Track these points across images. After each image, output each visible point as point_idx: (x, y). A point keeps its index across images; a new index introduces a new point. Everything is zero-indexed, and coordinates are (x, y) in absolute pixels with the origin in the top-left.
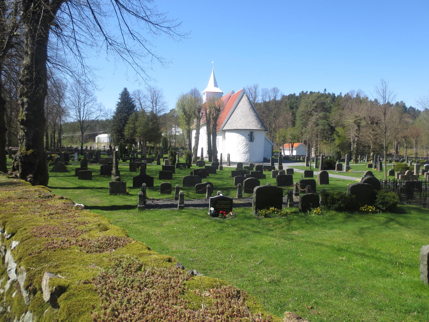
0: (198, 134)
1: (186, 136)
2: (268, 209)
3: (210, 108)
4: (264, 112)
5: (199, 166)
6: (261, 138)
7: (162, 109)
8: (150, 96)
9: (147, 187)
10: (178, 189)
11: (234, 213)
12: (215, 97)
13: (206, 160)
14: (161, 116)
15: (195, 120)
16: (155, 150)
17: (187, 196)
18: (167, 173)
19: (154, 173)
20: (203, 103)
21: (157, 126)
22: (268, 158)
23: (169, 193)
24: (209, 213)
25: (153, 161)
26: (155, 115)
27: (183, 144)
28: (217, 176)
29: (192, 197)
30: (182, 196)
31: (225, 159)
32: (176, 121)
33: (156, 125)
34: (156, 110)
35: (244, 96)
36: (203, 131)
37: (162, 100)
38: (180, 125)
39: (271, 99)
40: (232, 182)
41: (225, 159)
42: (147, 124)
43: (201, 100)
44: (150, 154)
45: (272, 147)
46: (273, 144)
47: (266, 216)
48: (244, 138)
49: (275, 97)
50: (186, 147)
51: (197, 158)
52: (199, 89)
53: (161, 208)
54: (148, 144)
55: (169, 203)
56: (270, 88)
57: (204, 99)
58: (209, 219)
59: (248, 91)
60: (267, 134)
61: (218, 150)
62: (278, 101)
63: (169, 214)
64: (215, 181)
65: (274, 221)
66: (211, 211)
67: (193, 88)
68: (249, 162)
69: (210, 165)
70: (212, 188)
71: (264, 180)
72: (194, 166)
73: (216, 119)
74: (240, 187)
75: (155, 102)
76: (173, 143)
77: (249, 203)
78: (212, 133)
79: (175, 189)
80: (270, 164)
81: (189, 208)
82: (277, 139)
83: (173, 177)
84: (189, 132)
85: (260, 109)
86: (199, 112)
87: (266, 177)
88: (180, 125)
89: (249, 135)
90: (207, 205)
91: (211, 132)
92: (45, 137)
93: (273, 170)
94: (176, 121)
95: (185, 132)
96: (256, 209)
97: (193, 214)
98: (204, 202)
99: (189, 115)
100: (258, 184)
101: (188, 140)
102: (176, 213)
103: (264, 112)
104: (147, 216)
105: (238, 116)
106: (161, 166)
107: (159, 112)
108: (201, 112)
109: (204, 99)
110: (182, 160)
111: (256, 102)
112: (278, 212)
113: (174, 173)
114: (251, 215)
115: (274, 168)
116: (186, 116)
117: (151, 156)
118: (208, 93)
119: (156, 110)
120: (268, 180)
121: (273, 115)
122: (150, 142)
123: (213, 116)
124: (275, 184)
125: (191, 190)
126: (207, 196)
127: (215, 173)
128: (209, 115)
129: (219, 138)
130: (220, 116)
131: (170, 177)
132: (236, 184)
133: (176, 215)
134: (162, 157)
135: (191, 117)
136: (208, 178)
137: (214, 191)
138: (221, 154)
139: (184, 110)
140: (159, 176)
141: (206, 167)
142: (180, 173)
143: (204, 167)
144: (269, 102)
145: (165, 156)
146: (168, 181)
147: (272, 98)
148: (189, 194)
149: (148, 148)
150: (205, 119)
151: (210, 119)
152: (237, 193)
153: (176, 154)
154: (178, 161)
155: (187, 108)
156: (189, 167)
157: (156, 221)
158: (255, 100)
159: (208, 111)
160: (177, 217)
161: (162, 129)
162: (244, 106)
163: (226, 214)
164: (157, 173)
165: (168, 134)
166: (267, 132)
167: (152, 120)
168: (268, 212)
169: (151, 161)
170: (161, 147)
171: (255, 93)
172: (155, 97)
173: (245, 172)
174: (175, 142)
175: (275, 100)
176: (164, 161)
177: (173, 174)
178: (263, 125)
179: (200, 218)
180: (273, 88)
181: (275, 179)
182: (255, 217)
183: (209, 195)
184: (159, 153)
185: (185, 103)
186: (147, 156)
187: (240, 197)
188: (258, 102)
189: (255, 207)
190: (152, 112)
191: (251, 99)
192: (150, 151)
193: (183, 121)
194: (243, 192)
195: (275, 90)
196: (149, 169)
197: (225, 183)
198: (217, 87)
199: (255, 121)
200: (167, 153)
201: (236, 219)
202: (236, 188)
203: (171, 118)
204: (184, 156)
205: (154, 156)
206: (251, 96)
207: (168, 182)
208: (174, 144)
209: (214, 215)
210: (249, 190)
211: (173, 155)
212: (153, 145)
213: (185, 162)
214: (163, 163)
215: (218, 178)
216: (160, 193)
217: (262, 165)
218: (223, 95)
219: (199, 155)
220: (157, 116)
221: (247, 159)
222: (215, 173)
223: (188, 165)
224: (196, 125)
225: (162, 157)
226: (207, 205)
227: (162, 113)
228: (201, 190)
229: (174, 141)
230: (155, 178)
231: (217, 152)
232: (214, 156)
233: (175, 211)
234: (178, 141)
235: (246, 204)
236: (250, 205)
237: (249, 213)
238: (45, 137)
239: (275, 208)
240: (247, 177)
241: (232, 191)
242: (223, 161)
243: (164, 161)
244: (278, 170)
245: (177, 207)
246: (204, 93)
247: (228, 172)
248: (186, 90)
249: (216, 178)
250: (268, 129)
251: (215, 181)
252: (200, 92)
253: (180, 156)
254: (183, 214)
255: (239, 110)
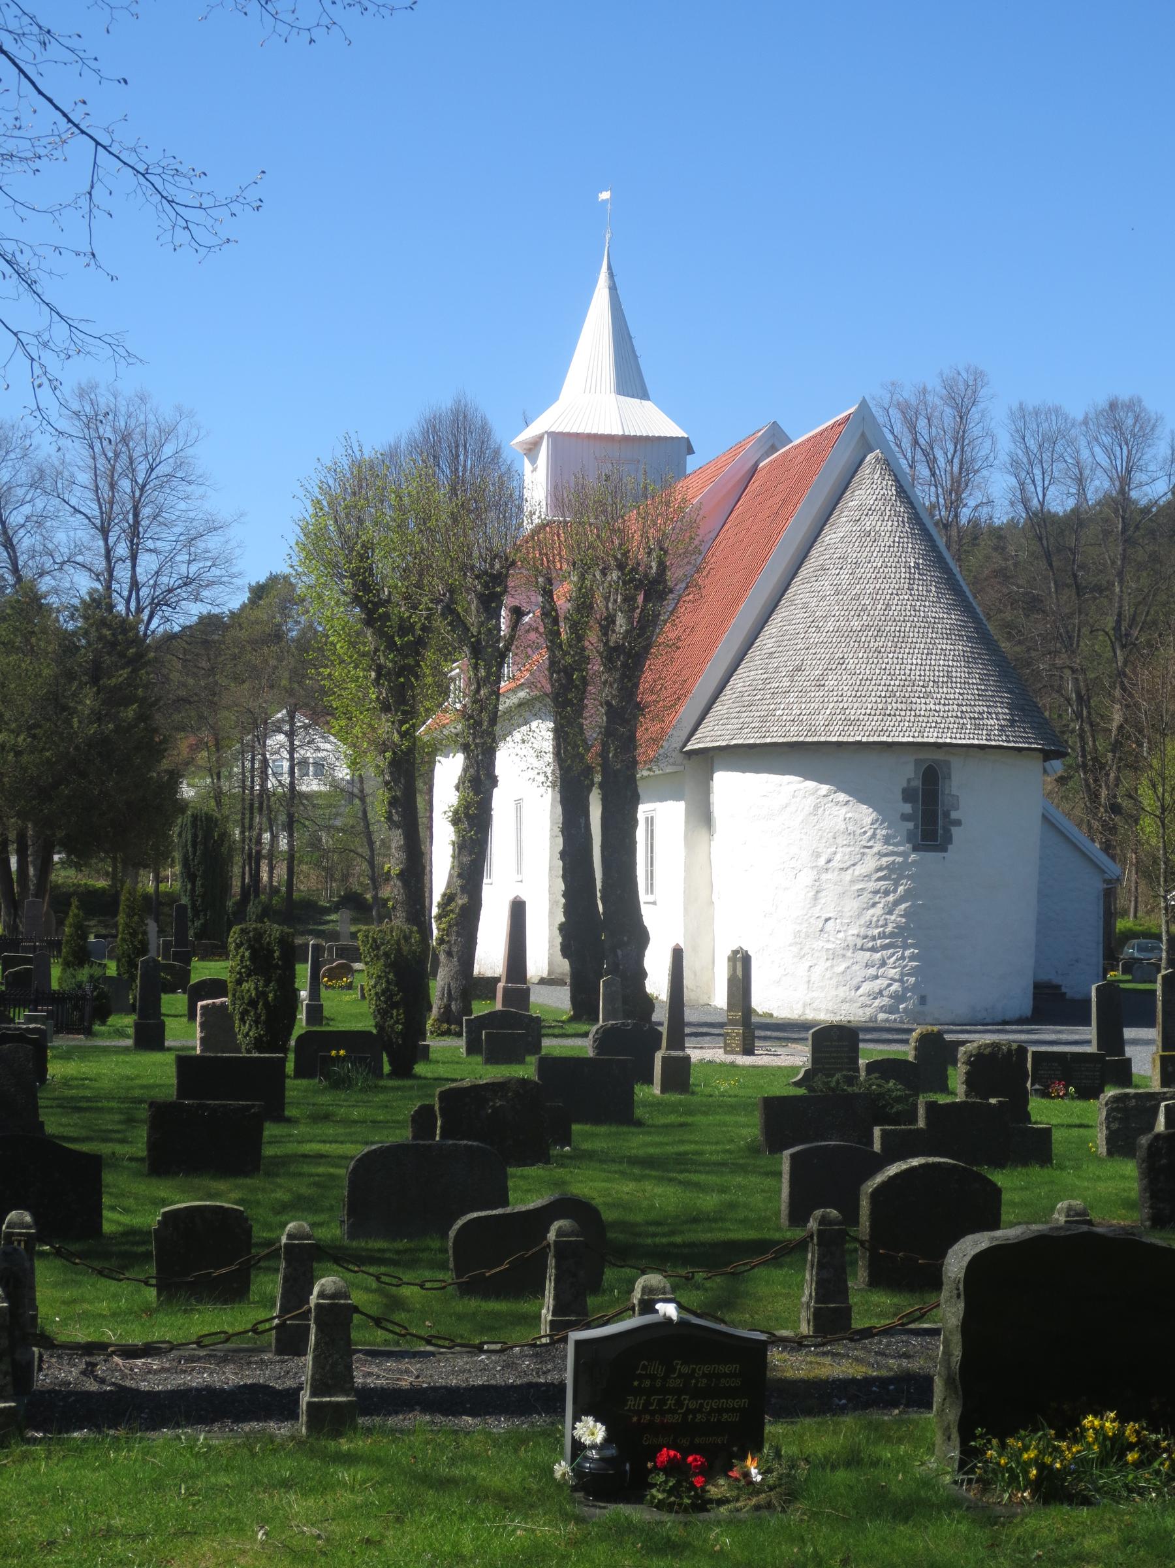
0: (480, 782)
1: (378, 808)
2: (1069, 1427)
3: (583, 568)
4: (1033, 604)
5: (491, 1060)
6: (1008, 817)
7: (187, 582)
8: (85, 478)
9: (40, 1238)
10: (304, 1260)
11: (780, 1469)
12: (611, 474)
13: (553, 1002)
14: (170, 637)
15: (458, 671)
16: (121, 918)
17: (378, 1322)
18: (215, 1118)
19: (109, 1122)
20: (528, 527)
21: (142, 717)
22: (1071, 990)
23: (233, 1290)
24: (562, 1469)
25: (102, 1014)
26: (125, 627)
27: (361, 867)
28: (637, 1143)
29: (425, 1328)
30: (337, 1317)
31: (714, 993)
32: (298, 676)
33: (130, 712)
34: (135, 585)
35: (865, 470)
36: (525, 766)
37: (183, 507)
38: (330, 712)
39: (1092, 497)
40: (769, 1193)
41: (714, 993)
42: (57, 704)
43: (508, 501)
44: (81, 956)
45: (1109, 894)
46: (1113, 869)
47: (1052, 1489)
48: (866, 815)
49: (1125, 481)
50: (386, 892)
51: (473, 986)
52: (491, 409)
53: (155, 1424)
54: (64, 875)
55: (229, 1377)
56: (1079, 399)
57: (536, 486)
58: (567, 1517)
59: (899, 427)
60: (1062, 780)
61: (650, 916)
62: (1146, 510)
63: (223, 1479)
64: (626, 1188)
65: (1113, 1538)
66: (578, 1446)
67: (444, 402)
68: (916, 1017)
69: (583, 1046)
70: (597, 1252)
71: (1036, 1173)
72: (449, 1058)
73: (629, 659)
74: (832, 1243)
75: (125, 518)
76: (277, 860)
77: (906, 1378)
78: (602, 786)
79: (275, 1254)
80: (1083, 1039)
81: (391, 1421)
82: (1148, 824)
83: (268, 1151)
84: (408, 775)
85: (1003, 575)
86: (490, 603)
87: (1057, 1148)
88: (330, 712)
89: (908, 795)
90: (541, 1400)
91: (589, 770)
92: (657, 1240)
93: (1110, 1092)
94: (298, 676)
95: (375, 767)
96: (966, 1431)
97: (425, 1480)
98: (525, 1370)
99: (405, 628)
100: (986, 1212)
101: (397, 838)
102: (285, 1468)
103: (1033, 604)
104: (38, 1490)
105: (815, 637)
106: (170, 1058)
107: (157, 604)
108: (508, 601)
109: (536, 486)
110: (350, 1006)
111: (965, 514)
112: (1150, 1452)
113: (281, 1119)
114: (926, 1483)
115: (1123, 1073)
116: (380, 633)
117: (83, 974)
118: (563, 443)
119: (135, 585)
120: (1068, 1177)
121: (1110, 622)
122: (80, 854)
123: (607, 643)
124: (1129, 1205)
125: (412, 1264)
126: (546, 1314)
127: (620, 1111)
128: (574, 627)
129: (661, 820)
130: (669, 633)
131: (237, 1152)
132: (798, 1215)
133: (286, 1484)
134: (179, 981)
135: (420, 643)
136: (562, 1161)
137: (609, 1274)
138: (678, 954)
139: (365, 586)
140: (152, 1146)
141: (549, 1065)
142: (326, 1117)
143: (527, 1070)
144: (1076, 520)
145: (203, 970)
146: (221, 1186)
147: (1099, 486)
148: (396, 1303)
149: (61, 900)
150: (541, 657)
151: (583, 660)
152: (807, 1292)
153: (292, 955)
154: (315, 1013)
155: (386, 570)
156: (403, 1069)
157: (109, 1533)
158: (955, 505)
159: (564, 595)
160: (297, 1504)
161: (183, 744)
162: (863, 550)
163: (709, 1473)
164: (130, 1121)
165: (231, 787)
166: (1057, 766)
167: (96, 673)
168: (1071, 1451)
169: (83, 1012)
170: (172, 898)
171: (959, 439)
172: (125, 484)
173: (877, 1109)
174: (291, 857)
175: (1120, 502)
176: (192, 1016)
177: (271, 1130)
178: (1024, 708)
179: (486, 1508)
180: (1102, 402)
181: (1130, 1169)
182: (954, 1503)
183: (572, 1311)
184: (155, 941)
185: (370, 532)
186: (56, 972)
187: (832, 1322)
188: (984, 512)
189: (953, 1415)
190: (99, 604)
191: (925, 495)
192: (81, 932)
193: (352, 680)
194: (858, 1280)
195: (1123, 424)
196: (66, 1082)
197: (709, 1202)
198: (644, 395)
199: (959, 674)
200: (218, 951)
201: (796, 1514)
202: (802, 1245)
203: (253, 654)
204: (364, 973)
205: (112, 969)
206: (923, 471)
207: (225, 1195)
208: (281, 871)
209: (608, 1482)
210: (907, 1266)
211: (272, 965)
212: (102, 883)
213: (368, 1024)
214: (186, 1034)
215: (650, 1163)
216: (151, 1294)
217: (1022, 1050)
218: (692, 463)
219: (490, 956)
220: (138, 641)
221: (898, 998)
222: (620, 1111)
223: (395, 1045)
224: (464, 715)
225: (179, 981)
226: (541, 1400)
227: (189, 613)
228: (500, 1262)
229: (283, 843)
230: (115, 1162)
231: (640, 937)
232: (614, 970)
233: (273, 1447)
234: (315, 843)
235: (882, 1382)
236: (911, 1391)
237: (903, 1464)
238: (657, 1240)
239: (1123, 1419)
240: (893, 1152)
241: (762, 1272)
242: (690, 1016)
243: (192, 1016)
244: (1156, 1086)
245: (293, 1415)
246: (532, 449)
247: (733, 1109)
248: (386, 425)
249: (634, 1161)
250: (1073, 740)
251: (626, 1188)
252: (498, 434)
253: (334, 974)
254: (344, 1475)
255: (825, 585)
